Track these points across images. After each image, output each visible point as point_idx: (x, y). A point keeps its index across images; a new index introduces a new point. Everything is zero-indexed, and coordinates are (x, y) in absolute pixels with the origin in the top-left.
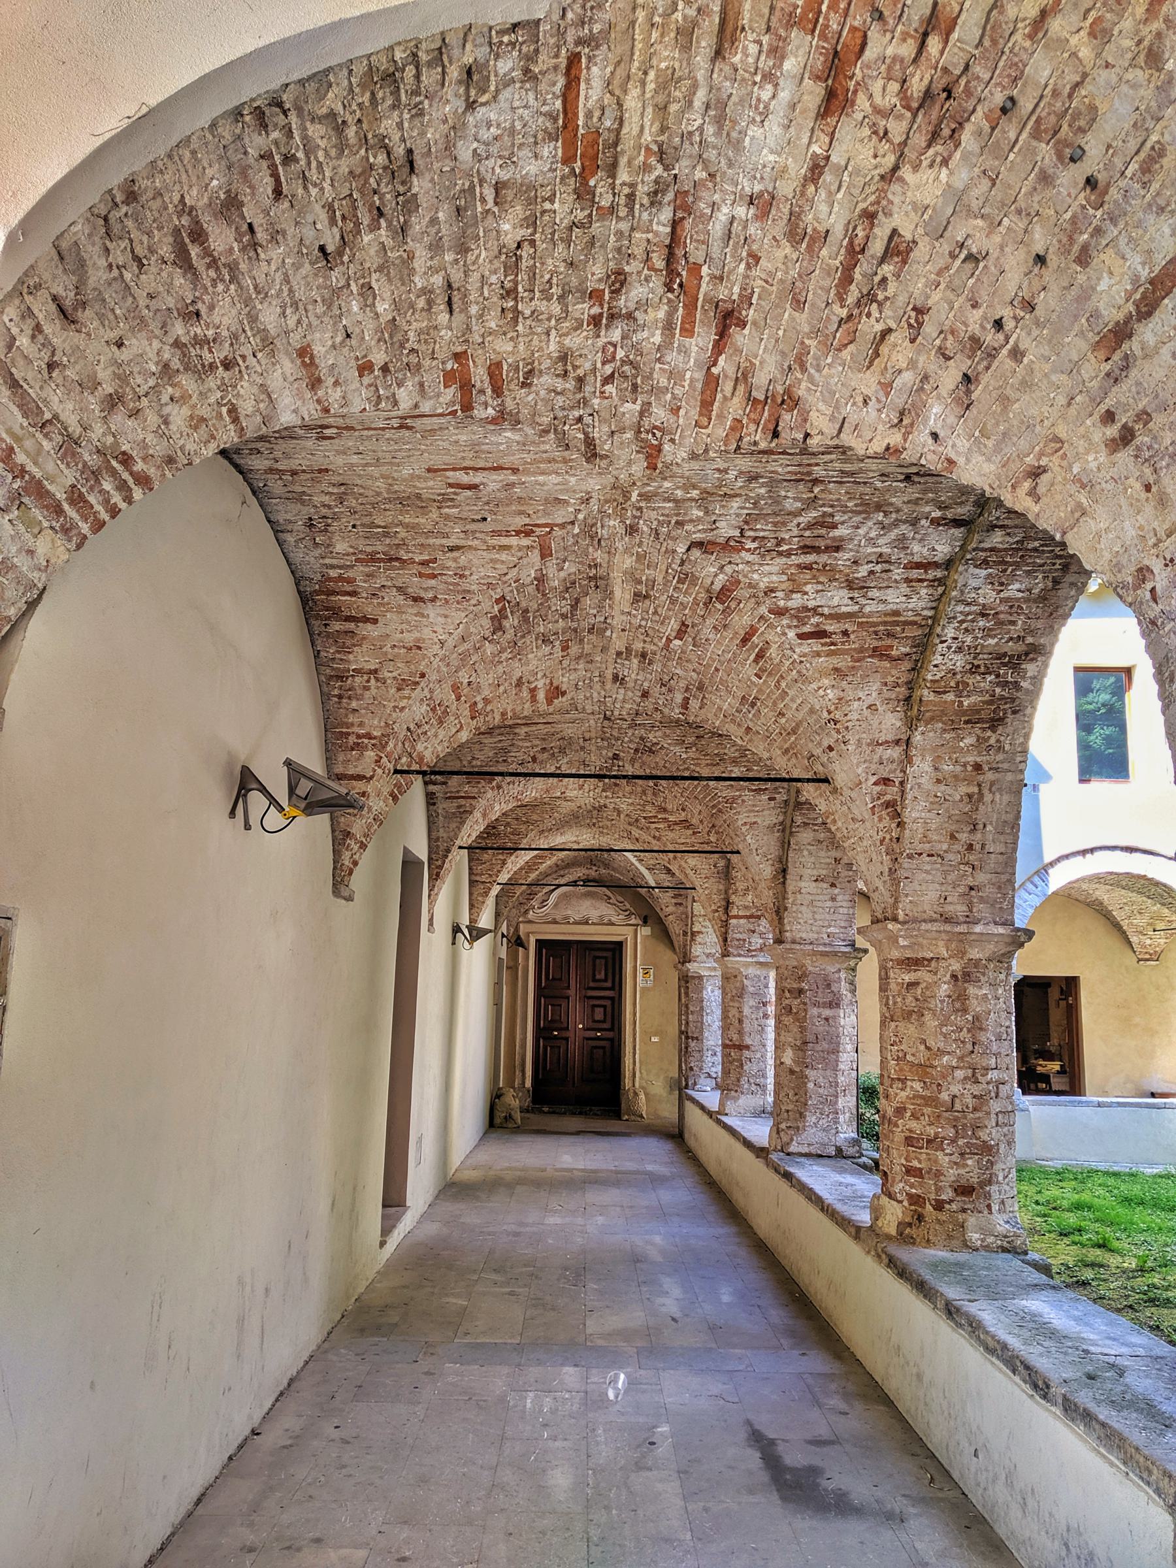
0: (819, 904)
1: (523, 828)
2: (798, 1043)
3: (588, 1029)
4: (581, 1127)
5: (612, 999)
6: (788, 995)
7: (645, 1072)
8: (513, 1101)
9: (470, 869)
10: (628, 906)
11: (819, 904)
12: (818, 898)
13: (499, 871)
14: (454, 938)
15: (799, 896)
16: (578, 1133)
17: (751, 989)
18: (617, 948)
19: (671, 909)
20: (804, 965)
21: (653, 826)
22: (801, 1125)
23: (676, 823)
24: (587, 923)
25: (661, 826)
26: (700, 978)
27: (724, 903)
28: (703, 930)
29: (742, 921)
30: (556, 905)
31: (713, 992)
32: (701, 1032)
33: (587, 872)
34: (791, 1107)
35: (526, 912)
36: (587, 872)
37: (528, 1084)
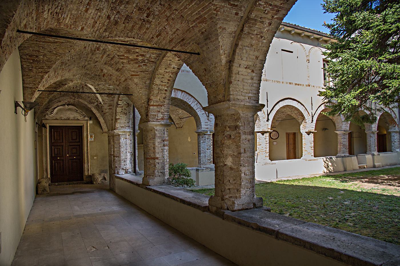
0: (246, 81)
1: (54, 57)
2: (235, 154)
3: (71, 156)
4: (73, 190)
5: (79, 145)
6: (228, 129)
7: (91, 166)
8: (45, 183)
9: (23, 80)
10: (84, 113)
11: (246, 81)
12: (246, 77)
13: (40, 82)
14: (16, 109)
15: (237, 76)
16: (73, 193)
17: (158, 135)
18: (80, 129)
19: (107, 111)
20: (239, 113)
21: (122, 60)
22: (238, 196)
23: (132, 60)
24: (69, 119)
25: (125, 61)
26: (119, 135)
27: (147, 100)
28: (120, 118)
29: (155, 107)
30: (57, 113)
31: (123, 140)
32: (120, 154)
33: (69, 100)
34: (231, 187)
35: (45, 116)
36: (69, 100)
37: (49, 176)
